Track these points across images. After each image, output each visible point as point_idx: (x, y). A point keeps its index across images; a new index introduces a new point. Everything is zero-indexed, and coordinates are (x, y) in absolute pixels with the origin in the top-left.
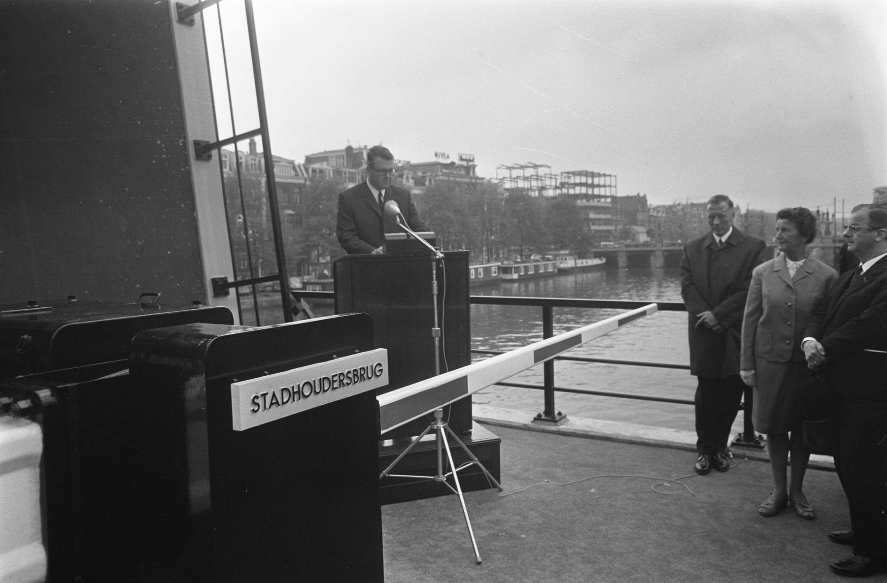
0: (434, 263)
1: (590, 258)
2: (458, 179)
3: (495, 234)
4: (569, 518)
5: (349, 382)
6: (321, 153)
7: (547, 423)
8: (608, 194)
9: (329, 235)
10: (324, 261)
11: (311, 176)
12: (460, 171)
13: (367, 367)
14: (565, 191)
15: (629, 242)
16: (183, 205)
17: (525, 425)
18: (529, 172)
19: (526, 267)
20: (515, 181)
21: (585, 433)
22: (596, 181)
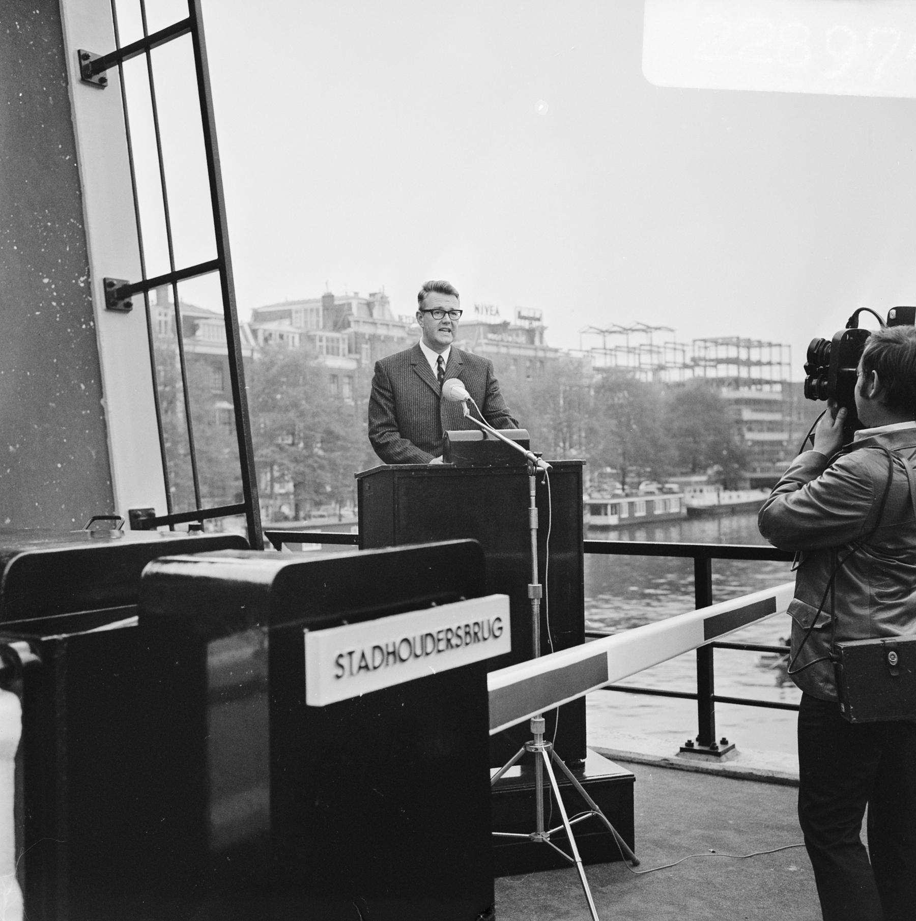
0: (533, 479)
1: (743, 489)
2: (514, 352)
3: (577, 447)
4: (757, 910)
6: (278, 305)
7: (704, 756)
8: (776, 377)
9: (293, 444)
10: (283, 491)
12: (517, 335)
13: (483, 622)
14: (699, 372)
16: (83, 387)
18: (636, 339)
19: (631, 504)
20: (611, 355)
21: (770, 775)
22: (755, 355)
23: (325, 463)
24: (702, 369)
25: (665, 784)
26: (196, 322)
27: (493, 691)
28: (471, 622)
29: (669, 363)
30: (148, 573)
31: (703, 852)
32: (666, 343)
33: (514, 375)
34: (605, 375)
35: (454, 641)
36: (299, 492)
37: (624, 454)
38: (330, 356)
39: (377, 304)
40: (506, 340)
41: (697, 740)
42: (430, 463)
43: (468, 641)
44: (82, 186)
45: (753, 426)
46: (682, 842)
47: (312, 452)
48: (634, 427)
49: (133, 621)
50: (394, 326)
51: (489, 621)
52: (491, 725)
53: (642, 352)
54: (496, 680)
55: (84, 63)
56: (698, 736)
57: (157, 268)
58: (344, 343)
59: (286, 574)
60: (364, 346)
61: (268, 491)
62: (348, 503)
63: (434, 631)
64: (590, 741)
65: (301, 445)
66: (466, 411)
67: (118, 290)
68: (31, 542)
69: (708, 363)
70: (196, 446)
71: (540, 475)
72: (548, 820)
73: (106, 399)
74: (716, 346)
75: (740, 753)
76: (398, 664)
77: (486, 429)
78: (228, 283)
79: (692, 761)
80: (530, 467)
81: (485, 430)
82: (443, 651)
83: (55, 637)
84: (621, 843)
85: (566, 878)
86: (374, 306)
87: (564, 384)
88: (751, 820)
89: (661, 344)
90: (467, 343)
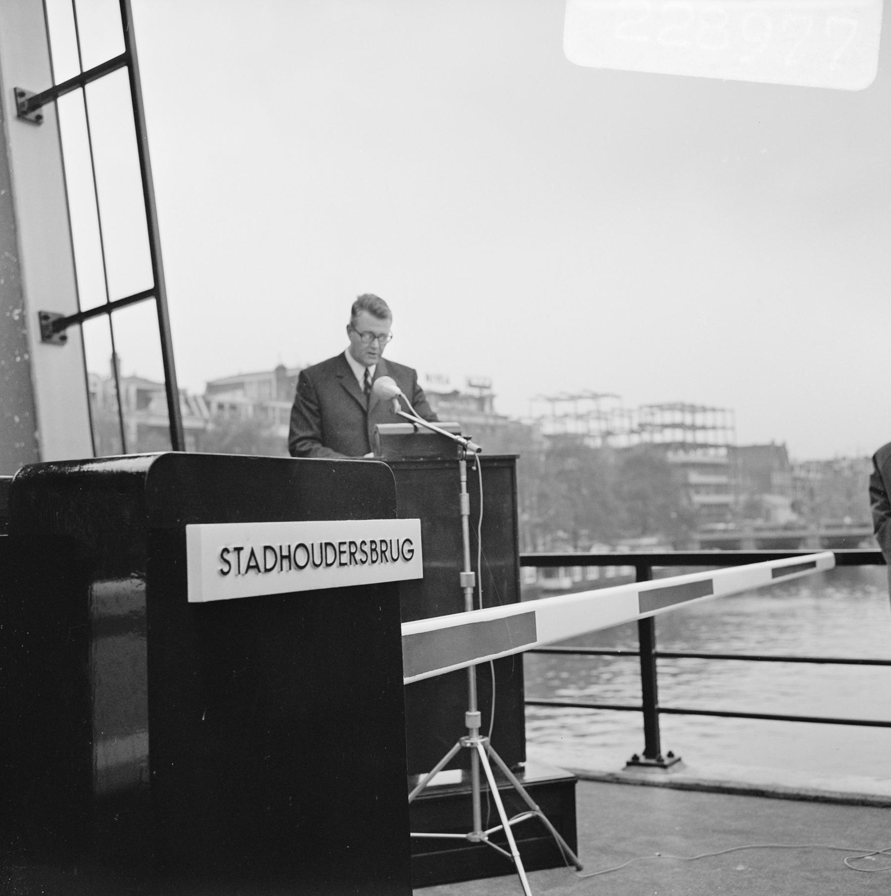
0: (463, 464)
5: (364, 560)
8: (721, 441)
14: (646, 437)
15: (760, 522)
17: (611, 775)
18: (584, 406)
22: (699, 419)
35: (359, 556)
43: (374, 559)
55: (21, 100)
71: (470, 461)
72: (487, 816)
82: (346, 564)
84: (563, 847)
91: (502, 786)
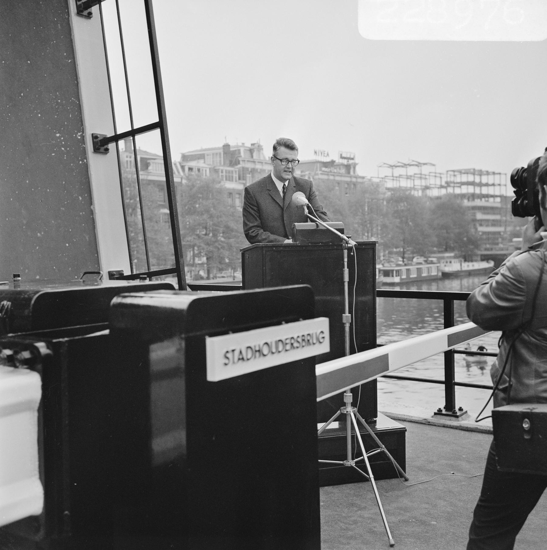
0: (346, 252)
1: (476, 261)
2: (338, 178)
3: (376, 236)
8: (497, 193)
9: (206, 234)
10: (200, 262)
11: (187, 175)
12: (340, 169)
14: (450, 190)
16: (80, 198)
18: (412, 171)
19: (408, 270)
20: (397, 180)
22: (484, 180)
23: (225, 245)
24: (452, 188)
25: (425, 434)
26: (148, 161)
27: (320, 376)
28: (306, 333)
29: (432, 185)
30: (115, 303)
31: (447, 473)
32: (430, 173)
33: (338, 193)
34: (393, 192)
35: (296, 345)
36: (210, 262)
37: (404, 240)
38: (228, 182)
39: (255, 150)
40: (333, 171)
41: (444, 408)
42: (284, 242)
44: (78, 78)
45: (483, 223)
46: (435, 468)
47: (217, 239)
48: (410, 223)
49: (106, 332)
50: (266, 163)
51: (316, 333)
52: (318, 396)
53: (416, 178)
54: (321, 369)
56: (445, 406)
57: (123, 127)
58: (236, 174)
59: (194, 304)
60: (248, 175)
61: (191, 262)
62: (239, 269)
63: (283, 339)
64: (380, 408)
65: (211, 235)
66: (306, 211)
67: (100, 140)
68: (48, 286)
69: (456, 185)
70: (148, 235)
71: (350, 249)
73: (94, 205)
74: (461, 174)
75: (470, 416)
76: (262, 358)
77: (318, 222)
78: (165, 136)
79: (441, 420)
80: (344, 244)
81: (317, 223)
83: (61, 340)
84: (397, 468)
85: (365, 488)
86: (254, 151)
87: (368, 198)
88: (476, 455)
89: (427, 173)
90: (309, 173)
91: (362, 433)
